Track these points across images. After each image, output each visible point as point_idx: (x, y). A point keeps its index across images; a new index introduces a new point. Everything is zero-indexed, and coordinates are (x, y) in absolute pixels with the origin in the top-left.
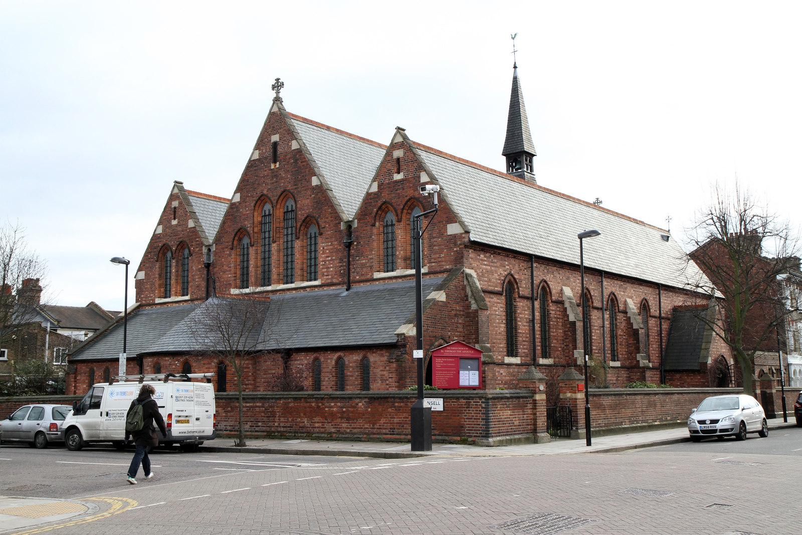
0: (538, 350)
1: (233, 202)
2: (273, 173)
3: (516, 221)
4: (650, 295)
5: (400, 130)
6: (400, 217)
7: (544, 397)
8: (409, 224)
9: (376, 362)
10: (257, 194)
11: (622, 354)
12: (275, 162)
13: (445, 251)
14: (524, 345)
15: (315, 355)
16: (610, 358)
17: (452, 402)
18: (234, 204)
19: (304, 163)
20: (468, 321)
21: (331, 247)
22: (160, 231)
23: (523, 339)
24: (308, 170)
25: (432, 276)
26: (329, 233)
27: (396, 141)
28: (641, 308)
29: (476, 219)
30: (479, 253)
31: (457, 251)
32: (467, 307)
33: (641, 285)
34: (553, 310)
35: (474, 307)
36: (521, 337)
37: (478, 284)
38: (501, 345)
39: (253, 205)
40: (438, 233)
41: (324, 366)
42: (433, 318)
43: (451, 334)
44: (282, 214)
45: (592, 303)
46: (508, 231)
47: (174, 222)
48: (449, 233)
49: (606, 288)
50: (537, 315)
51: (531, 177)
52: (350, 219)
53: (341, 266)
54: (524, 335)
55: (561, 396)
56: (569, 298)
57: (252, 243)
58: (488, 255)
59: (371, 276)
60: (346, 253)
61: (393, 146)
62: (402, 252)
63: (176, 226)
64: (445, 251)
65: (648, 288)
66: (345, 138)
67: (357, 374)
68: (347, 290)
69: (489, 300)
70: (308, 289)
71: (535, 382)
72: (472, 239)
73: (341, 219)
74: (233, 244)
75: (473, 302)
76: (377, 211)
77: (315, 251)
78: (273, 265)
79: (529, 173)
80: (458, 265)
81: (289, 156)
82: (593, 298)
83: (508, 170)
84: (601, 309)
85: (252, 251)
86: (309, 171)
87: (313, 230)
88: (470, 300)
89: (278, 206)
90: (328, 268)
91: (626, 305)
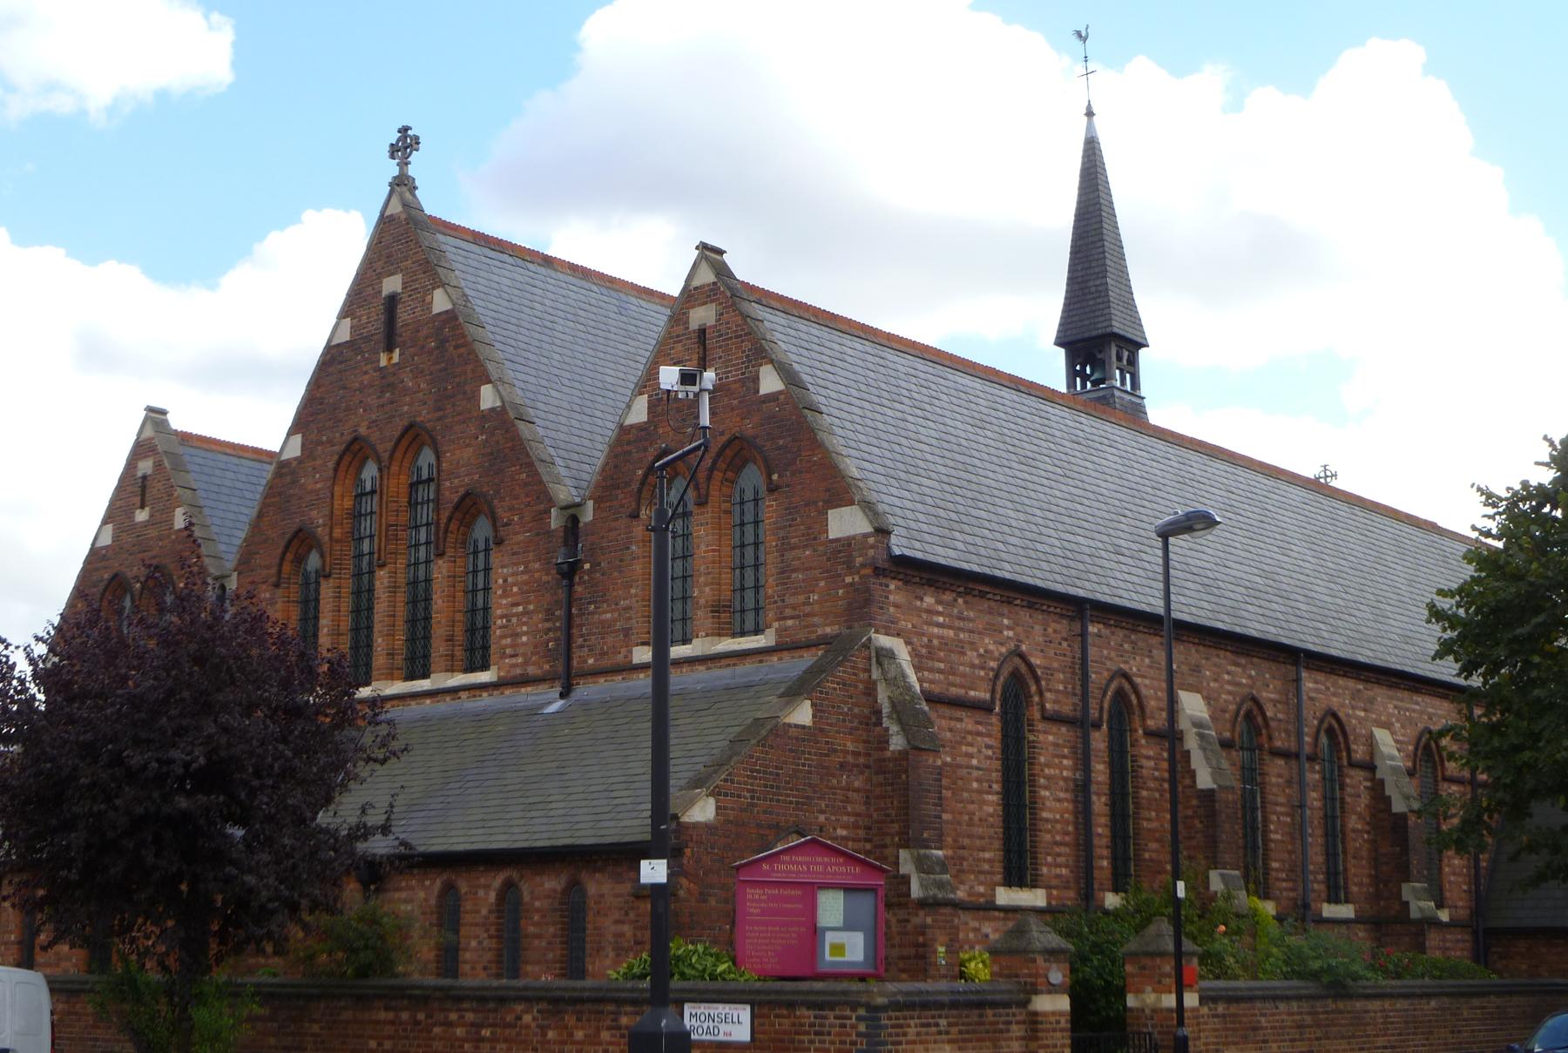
0: (1102, 868)
1: (282, 458)
2: (383, 378)
3: (1045, 506)
4: (1268, 685)
5: (709, 254)
6: (703, 492)
7: (1063, 1003)
8: (727, 512)
9: (602, 896)
10: (342, 434)
11: (1360, 884)
12: (389, 349)
13: (822, 584)
14: (1059, 855)
15: (445, 876)
16: (1324, 895)
17: (777, 1016)
18: (287, 463)
19: (462, 350)
20: (881, 785)
21: (525, 577)
22: (106, 540)
23: (1053, 837)
24: (471, 366)
25: (786, 655)
26: (520, 538)
27: (696, 283)
28: (1415, 755)
29: (917, 497)
30: (919, 591)
31: (851, 584)
32: (879, 742)
33: (1417, 691)
34: (1149, 758)
35: (897, 742)
36: (1049, 831)
37: (912, 677)
38: (987, 855)
39: (331, 465)
40: (803, 535)
41: (468, 906)
42: (771, 773)
43: (826, 819)
44: (404, 490)
45: (1270, 738)
46: (1017, 532)
47: (142, 516)
48: (831, 536)
49: (1311, 699)
50: (1100, 771)
51: (1132, 403)
52: (578, 500)
53: (549, 630)
54: (1058, 826)
55: (1131, 1001)
56: (1198, 724)
57: (327, 569)
58: (948, 597)
59: (626, 657)
60: (562, 594)
61: (689, 296)
62: (707, 589)
63: (146, 524)
64: (822, 584)
65: (1437, 702)
66: (595, 288)
67: (551, 929)
68: (562, 696)
69: (943, 724)
70: (464, 695)
71: (1034, 961)
72: (897, 551)
73: (551, 502)
74: (280, 571)
75: (894, 728)
76: (646, 476)
77: (486, 589)
78: (377, 627)
79: (1126, 392)
80: (856, 625)
81: (424, 332)
82: (1273, 724)
83: (1071, 384)
84: (1297, 756)
85: (327, 590)
86: (473, 371)
87: (482, 530)
88: (886, 722)
89: (395, 468)
90: (516, 635)
91: (1371, 745)
